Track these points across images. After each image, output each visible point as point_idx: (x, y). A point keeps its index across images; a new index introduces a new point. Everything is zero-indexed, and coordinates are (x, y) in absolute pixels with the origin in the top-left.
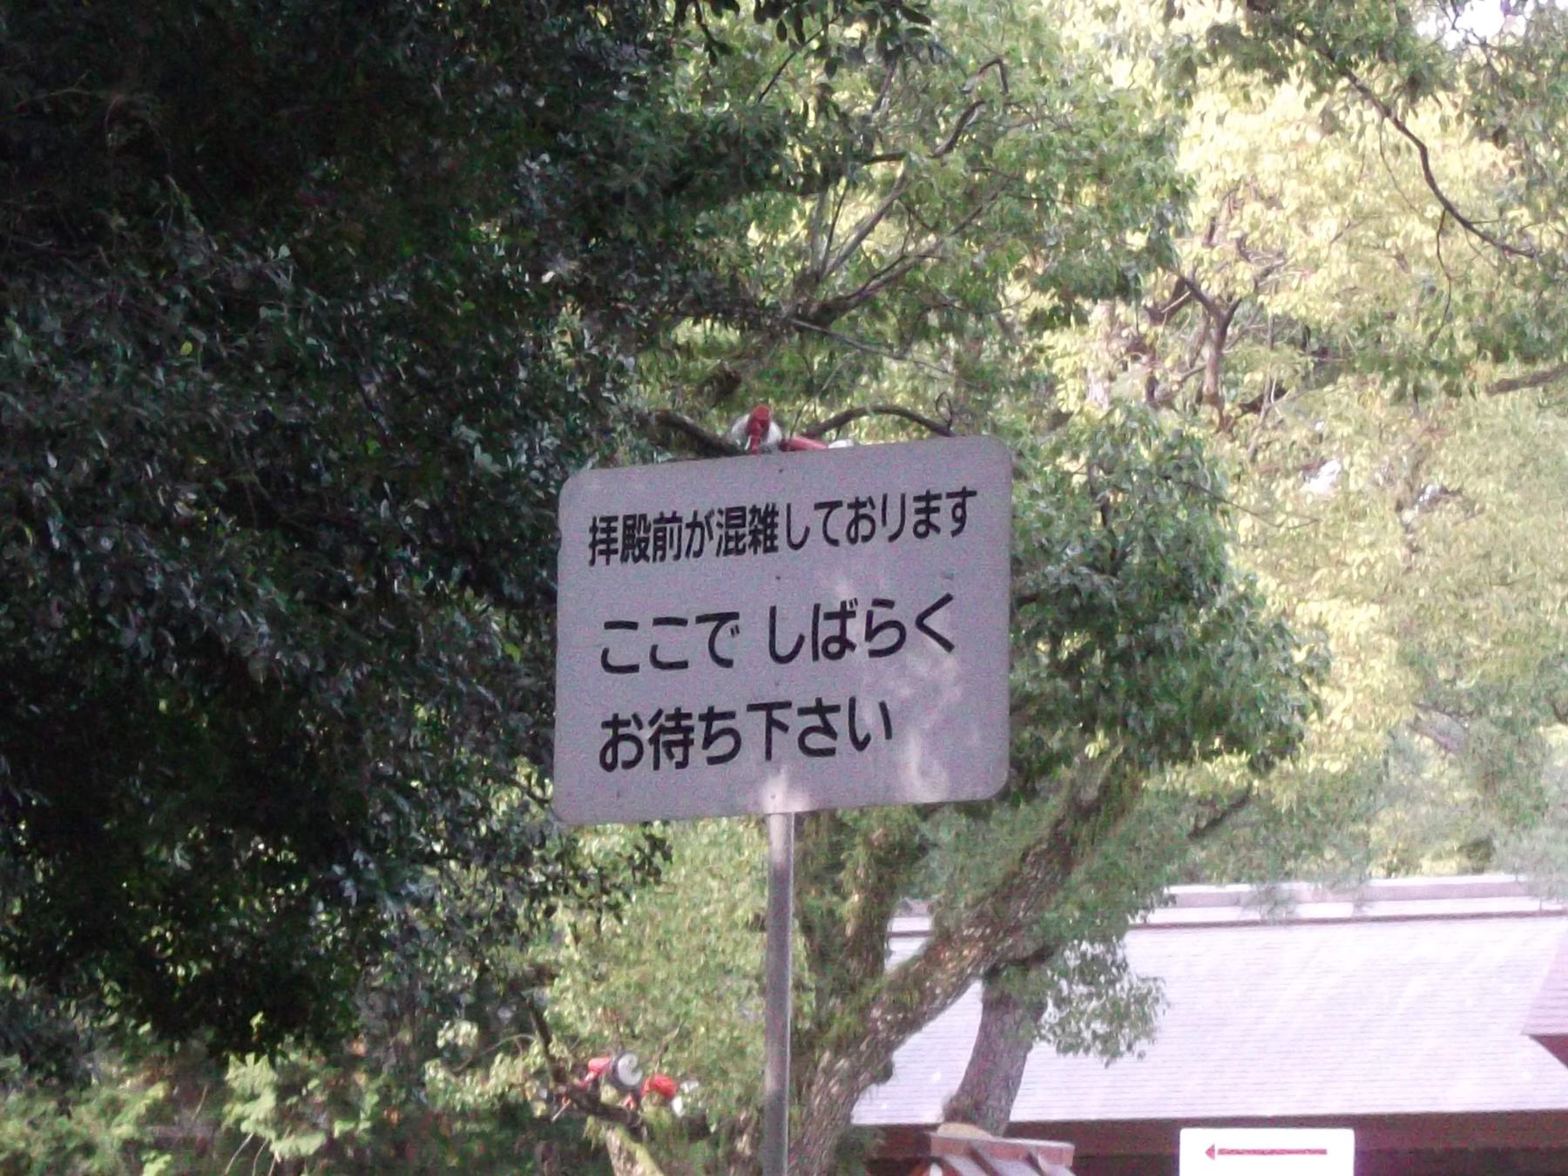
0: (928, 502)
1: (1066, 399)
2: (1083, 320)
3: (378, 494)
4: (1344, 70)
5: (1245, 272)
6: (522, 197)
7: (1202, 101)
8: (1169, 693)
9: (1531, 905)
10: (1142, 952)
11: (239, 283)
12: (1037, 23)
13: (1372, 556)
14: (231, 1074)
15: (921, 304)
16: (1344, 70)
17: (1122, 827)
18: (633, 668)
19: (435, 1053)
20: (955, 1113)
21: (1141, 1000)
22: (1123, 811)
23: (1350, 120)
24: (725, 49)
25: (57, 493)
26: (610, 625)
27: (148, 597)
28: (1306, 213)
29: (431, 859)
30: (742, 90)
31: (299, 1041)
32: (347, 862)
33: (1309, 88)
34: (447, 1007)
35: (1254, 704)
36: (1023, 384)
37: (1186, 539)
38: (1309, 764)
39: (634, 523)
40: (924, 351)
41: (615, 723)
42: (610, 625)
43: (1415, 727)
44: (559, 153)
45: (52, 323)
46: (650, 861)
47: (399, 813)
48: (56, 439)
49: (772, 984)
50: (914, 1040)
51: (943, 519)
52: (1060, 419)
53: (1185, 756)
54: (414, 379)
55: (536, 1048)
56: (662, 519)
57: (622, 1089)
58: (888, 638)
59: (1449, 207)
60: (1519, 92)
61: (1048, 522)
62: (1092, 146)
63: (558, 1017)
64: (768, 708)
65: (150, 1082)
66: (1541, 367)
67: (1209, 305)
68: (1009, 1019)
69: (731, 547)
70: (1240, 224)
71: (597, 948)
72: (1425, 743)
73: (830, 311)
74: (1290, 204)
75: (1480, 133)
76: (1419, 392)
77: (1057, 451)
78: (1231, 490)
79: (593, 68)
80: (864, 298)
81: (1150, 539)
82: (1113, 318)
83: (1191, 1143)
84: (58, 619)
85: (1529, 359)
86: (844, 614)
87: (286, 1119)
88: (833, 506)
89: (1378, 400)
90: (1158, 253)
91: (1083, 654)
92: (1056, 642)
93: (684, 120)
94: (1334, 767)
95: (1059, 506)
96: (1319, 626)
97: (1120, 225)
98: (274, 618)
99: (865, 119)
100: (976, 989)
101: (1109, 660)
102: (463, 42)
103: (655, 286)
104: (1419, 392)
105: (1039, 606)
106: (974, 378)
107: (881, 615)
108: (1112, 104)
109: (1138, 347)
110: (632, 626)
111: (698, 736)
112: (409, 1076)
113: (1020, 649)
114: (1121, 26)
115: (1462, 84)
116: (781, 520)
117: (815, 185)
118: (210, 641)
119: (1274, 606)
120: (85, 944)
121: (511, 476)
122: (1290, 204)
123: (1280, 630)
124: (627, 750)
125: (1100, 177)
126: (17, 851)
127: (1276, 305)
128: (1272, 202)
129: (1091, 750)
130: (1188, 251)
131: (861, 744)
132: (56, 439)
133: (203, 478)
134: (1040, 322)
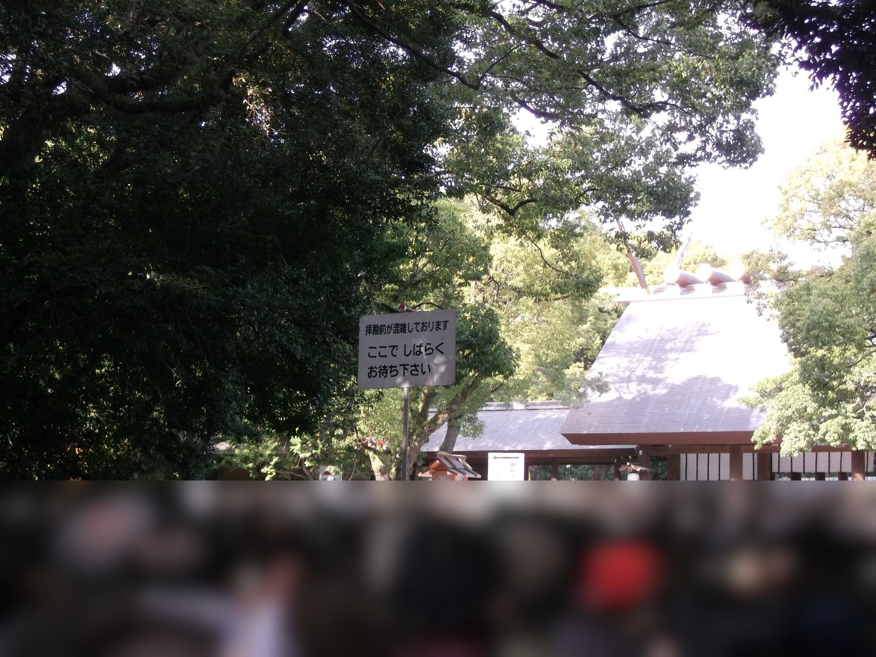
0: (438, 323)
1: (466, 301)
3: (324, 320)
5: (504, 276)
6: (354, 258)
7: (494, 240)
8: (487, 362)
10: (480, 415)
12: (461, 223)
15: (436, 281)
17: (477, 390)
19: (334, 436)
20: (441, 449)
22: (476, 387)
23: (525, 244)
25: (257, 319)
28: (516, 265)
29: (334, 396)
30: (399, 236)
36: (457, 298)
37: (491, 330)
38: (516, 377)
39: (375, 326)
40: (436, 291)
44: (362, 249)
46: (379, 397)
48: (256, 308)
49: (405, 421)
50: (433, 434)
51: (442, 327)
52: (465, 305)
53: (490, 376)
57: (373, 444)
59: (546, 262)
60: (561, 238)
61: (462, 326)
64: (404, 365)
70: (504, 266)
73: (419, 282)
74: (513, 262)
75: (553, 247)
79: (369, 231)
80: (424, 280)
83: (491, 456)
84: (257, 346)
86: (420, 346)
87: (303, 450)
89: (530, 302)
90: (486, 271)
91: (470, 354)
92: (464, 352)
94: (521, 378)
96: (518, 349)
97: (478, 265)
98: (302, 346)
100: (446, 423)
105: (462, 344)
106: (448, 296)
107: (428, 346)
109: (481, 290)
112: (329, 441)
113: (457, 352)
114: (478, 224)
117: (415, 257)
118: (289, 350)
119: (509, 344)
120: (262, 413)
121: (351, 317)
122: (513, 262)
123: (510, 349)
124: (374, 374)
125: (473, 255)
127: (509, 283)
128: (509, 262)
129: (471, 374)
130: (492, 272)
131: (424, 373)
132: (256, 308)
134: (461, 285)
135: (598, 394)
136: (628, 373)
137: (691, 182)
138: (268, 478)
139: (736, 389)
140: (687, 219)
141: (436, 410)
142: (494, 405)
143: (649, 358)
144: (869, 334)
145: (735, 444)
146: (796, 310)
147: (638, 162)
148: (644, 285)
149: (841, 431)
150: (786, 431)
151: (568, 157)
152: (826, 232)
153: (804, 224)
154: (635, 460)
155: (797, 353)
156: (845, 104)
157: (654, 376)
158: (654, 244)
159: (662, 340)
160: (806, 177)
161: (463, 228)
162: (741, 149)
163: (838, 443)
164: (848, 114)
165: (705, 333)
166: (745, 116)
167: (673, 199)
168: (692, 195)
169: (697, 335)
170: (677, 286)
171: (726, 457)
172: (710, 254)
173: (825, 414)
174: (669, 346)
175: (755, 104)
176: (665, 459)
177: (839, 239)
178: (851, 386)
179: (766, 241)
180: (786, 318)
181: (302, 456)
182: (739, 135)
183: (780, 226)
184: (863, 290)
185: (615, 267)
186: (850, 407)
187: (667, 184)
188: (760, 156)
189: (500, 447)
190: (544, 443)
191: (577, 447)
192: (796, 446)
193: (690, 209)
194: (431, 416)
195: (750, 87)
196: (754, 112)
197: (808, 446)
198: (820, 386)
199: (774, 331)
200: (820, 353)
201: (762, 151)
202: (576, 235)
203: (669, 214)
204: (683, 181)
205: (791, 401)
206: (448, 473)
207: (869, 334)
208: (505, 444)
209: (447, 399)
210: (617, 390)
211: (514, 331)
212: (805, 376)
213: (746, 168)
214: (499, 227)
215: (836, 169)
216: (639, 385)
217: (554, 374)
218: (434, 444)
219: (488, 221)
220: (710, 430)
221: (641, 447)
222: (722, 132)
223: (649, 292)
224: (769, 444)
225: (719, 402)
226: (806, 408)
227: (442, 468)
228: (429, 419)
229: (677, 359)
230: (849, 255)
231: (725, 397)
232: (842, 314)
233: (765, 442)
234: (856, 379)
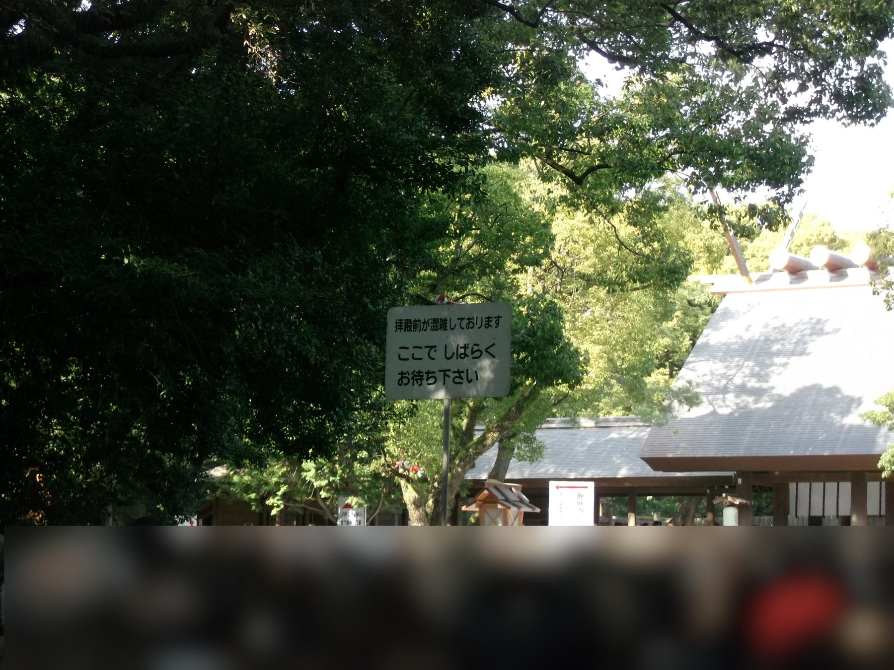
1: (522, 291)
2: (526, 271)
3: (344, 316)
4: (594, 207)
5: (569, 260)
7: (557, 215)
8: (549, 368)
9: (641, 424)
10: (539, 434)
11: (307, 261)
12: (515, 194)
13: (600, 333)
14: (303, 464)
16: (594, 207)
18: (407, 359)
19: (356, 459)
21: (539, 448)
22: (534, 399)
23: (596, 221)
24: (435, 201)
26: (401, 348)
27: (284, 341)
28: (585, 246)
29: (356, 409)
30: (438, 211)
31: (322, 457)
32: (334, 410)
33: (586, 211)
34: (360, 447)
35: (570, 370)
36: (510, 288)
37: (552, 328)
38: (584, 387)
39: (408, 321)
40: (484, 279)
41: (402, 373)
42: (401, 348)
43: (611, 377)
44: (391, 227)
45: (259, 270)
46: (413, 412)
47: (348, 398)
50: (480, 457)
51: (493, 323)
52: (520, 296)
54: (353, 286)
55: (383, 459)
56: (415, 321)
57: (405, 469)
58: (478, 354)
60: (640, 213)
61: (516, 324)
62: (529, 226)
63: (388, 451)
64: (444, 371)
65: (282, 466)
66: (645, 284)
67: (559, 267)
68: (505, 452)
69: (434, 329)
70: (569, 247)
71: (399, 433)
72: (613, 382)
75: (630, 223)
76: (614, 291)
77: (519, 305)
78: (564, 316)
79: (400, 204)
80: (469, 265)
81: (543, 328)
82: (534, 270)
83: (552, 485)
85: (642, 282)
87: (318, 477)
88: (463, 319)
89: (602, 292)
90: (547, 255)
93: (423, 219)
94: (590, 387)
95: (520, 319)
96: (586, 351)
98: (316, 347)
99: (470, 219)
101: (532, 359)
102: (366, 199)
103: (415, 262)
104: (614, 291)
105: (519, 345)
107: (476, 348)
108: (535, 216)
109: (541, 278)
110: (407, 348)
111: (425, 377)
112: (350, 466)
114: (537, 195)
115: (625, 211)
116: (448, 322)
117: (457, 236)
119: (575, 345)
120: (266, 431)
124: (405, 381)
126: (249, 407)
128: (575, 242)
129: (527, 383)
130: (554, 255)
133: (298, 310)
134: (515, 271)
135: (686, 407)
136: (724, 382)
137: (803, 143)
138: (274, 512)
139: (859, 402)
140: (798, 189)
141: (483, 427)
143: (751, 364)
148: (744, 272)
154: (733, 490)
157: (757, 385)
158: (757, 220)
165: (821, 333)
166: (870, 60)
167: (780, 165)
168: (804, 159)
169: (811, 334)
170: (786, 273)
171: (846, 487)
174: (775, 348)
176: (771, 489)
181: (316, 484)
182: (863, 82)
185: (709, 249)
189: (564, 473)
191: (660, 474)
193: (802, 176)
194: (477, 436)
196: (881, 55)
203: (775, 183)
204: (793, 141)
206: (499, 506)
208: (570, 471)
209: (498, 414)
210: (710, 403)
211: (582, 330)
213: (872, 125)
214: (563, 199)
216: (737, 397)
221: (741, 474)
222: (842, 80)
223: (750, 281)
225: (837, 418)
227: (491, 500)
228: (475, 439)
229: (785, 365)
231: (846, 412)
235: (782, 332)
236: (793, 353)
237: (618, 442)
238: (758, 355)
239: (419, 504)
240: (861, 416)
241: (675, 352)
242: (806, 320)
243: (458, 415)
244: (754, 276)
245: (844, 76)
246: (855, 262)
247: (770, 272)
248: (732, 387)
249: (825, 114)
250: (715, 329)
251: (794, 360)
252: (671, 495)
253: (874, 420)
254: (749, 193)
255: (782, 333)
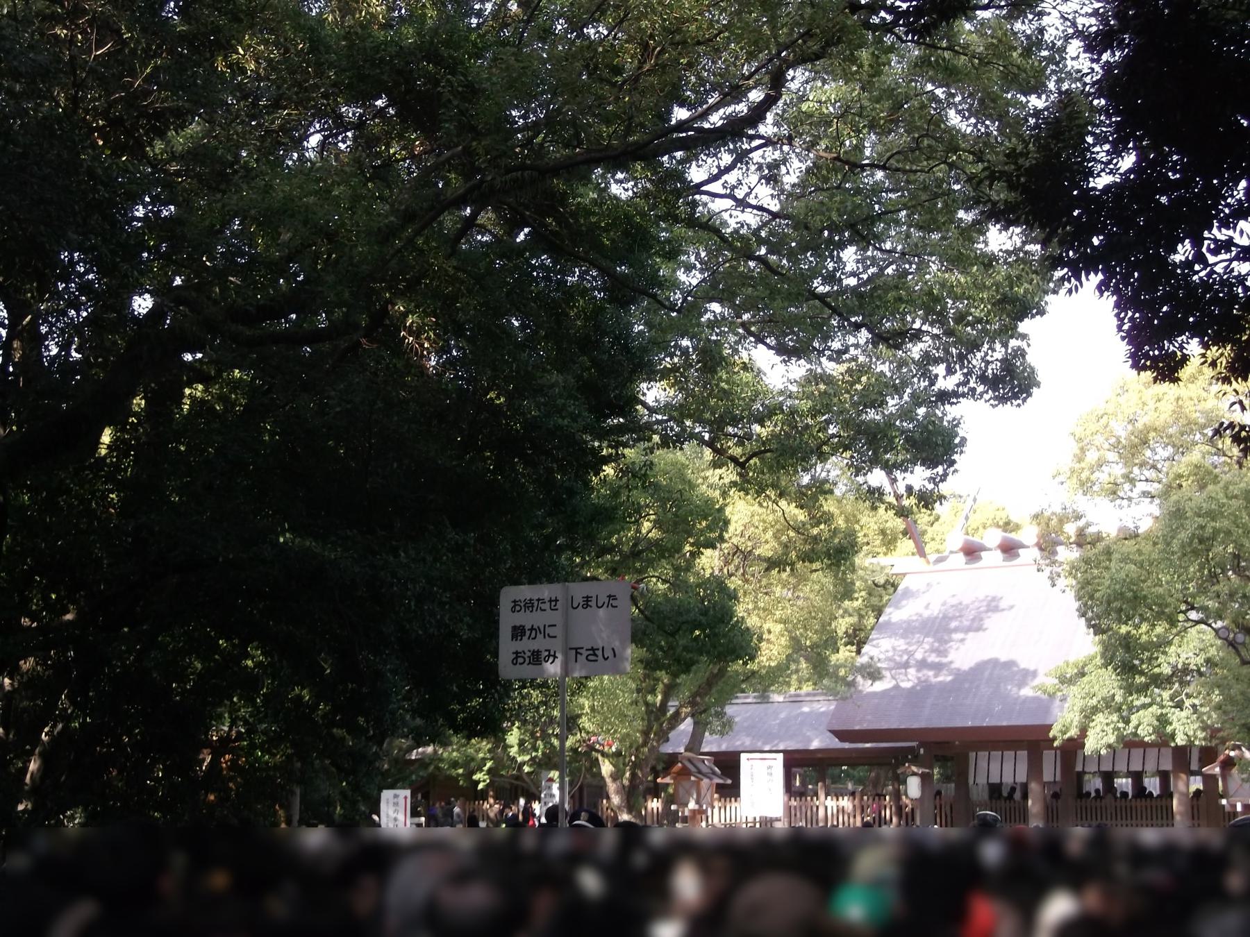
5: (750, 544)
8: (721, 645)
10: (729, 710)
22: (723, 676)
28: (765, 530)
35: (742, 647)
37: (723, 607)
64: (576, 649)
73: (641, 552)
83: (743, 756)
124: (520, 660)
131: (606, 659)
135: (870, 682)
136: (905, 657)
137: (956, 423)
138: (480, 786)
139: (1034, 674)
140: (952, 469)
141: (677, 703)
142: (751, 697)
143: (930, 640)
144: (1183, 608)
145: (1031, 741)
146: (1094, 578)
147: (894, 402)
148: (921, 552)
149: (1156, 723)
150: (1091, 725)
151: (808, 398)
152: (1127, 486)
153: (1103, 477)
154: (916, 760)
155: (1098, 630)
156: (1122, 315)
157: (937, 660)
158: (913, 501)
159: (945, 617)
160: (1104, 421)
161: (692, 486)
162: (1013, 383)
163: (1153, 737)
164: (1126, 327)
165: (996, 609)
166: (1013, 343)
167: (936, 447)
168: (957, 441)
169: (987, 611)
170: (961, 554)
171: (1023, 754)
172: (1001, 517)
173: (1137, 703)
174: (953, 624)
175: (1024, 326)
176: (952, 758)
177: (1145, 494)
178: (1167, 670)
179: (1057, 498)
180: (1083, 588)
181: (519, 759)
182: (1007, 364)
183: (1075, 480)
184: (1173, 553)
185: (883, 532)
186: (1166, 695)
187: (926, 427)
188: (1035, 390)
189: (759, 745)
190: (810, 741)
191: (847, 745)
192: (1103, 742)
193: (955, 457)
194: (672, 711)
195: (1017, 308)
196: (1024, 337)
197: (1117, 742)
198: (1127, 670)
199: (1070, 603)
200: (1124, 629)
201: (1038, 385)
202: (826, 493)
203: (930, 463)
204: (945, 423)
205: (1097, 688)
206: (693, 778)
207: (1183, 608)
208: (765, 743)
209: (690, 690)
210: (893, 678)
211: (764, 610)
212: (1108, 658)
213: (1019, 405)
214: (734, 484)
215: (1139, 412)
216: (918, 671)
217: (815, 655)
218: (679, 739)
219: (721, 478)
220: (1005, 724)
221: (922, 744)
222: (988, 363)
223: (928, 562)
224: (1071, 740)
225: (1015, 690)
226: (1114, 695)
227: (685, 773)
228: (668, 714)
229: (962, 640)
230: (1157, 512)
231: (1022, 684)
232: (1149, 583)
233: (1066, 737)
234: (1172, 660)
235: (960, 609)
236: (968, 630)
237: (809, 716)
238: (937, 631)
239: (616, 776)
240: (1034, 688)
241: (860, 630)
242: (981, 597)
243: (653, 691)
244: (932, 558)
245: (988, 358)
246: (1026, 543)
247: (946, 554)
248: (912, 662)
249: (973, 396)
250: (897, 608)
251: (971, 634)
252: (864, 765)
253: (1045, 692)
254: (908, 475)
255: (961, 610)
